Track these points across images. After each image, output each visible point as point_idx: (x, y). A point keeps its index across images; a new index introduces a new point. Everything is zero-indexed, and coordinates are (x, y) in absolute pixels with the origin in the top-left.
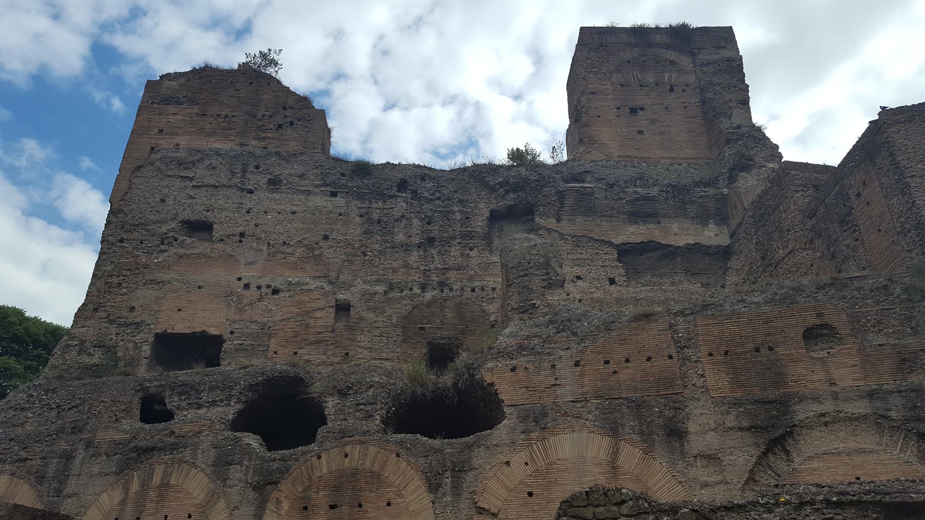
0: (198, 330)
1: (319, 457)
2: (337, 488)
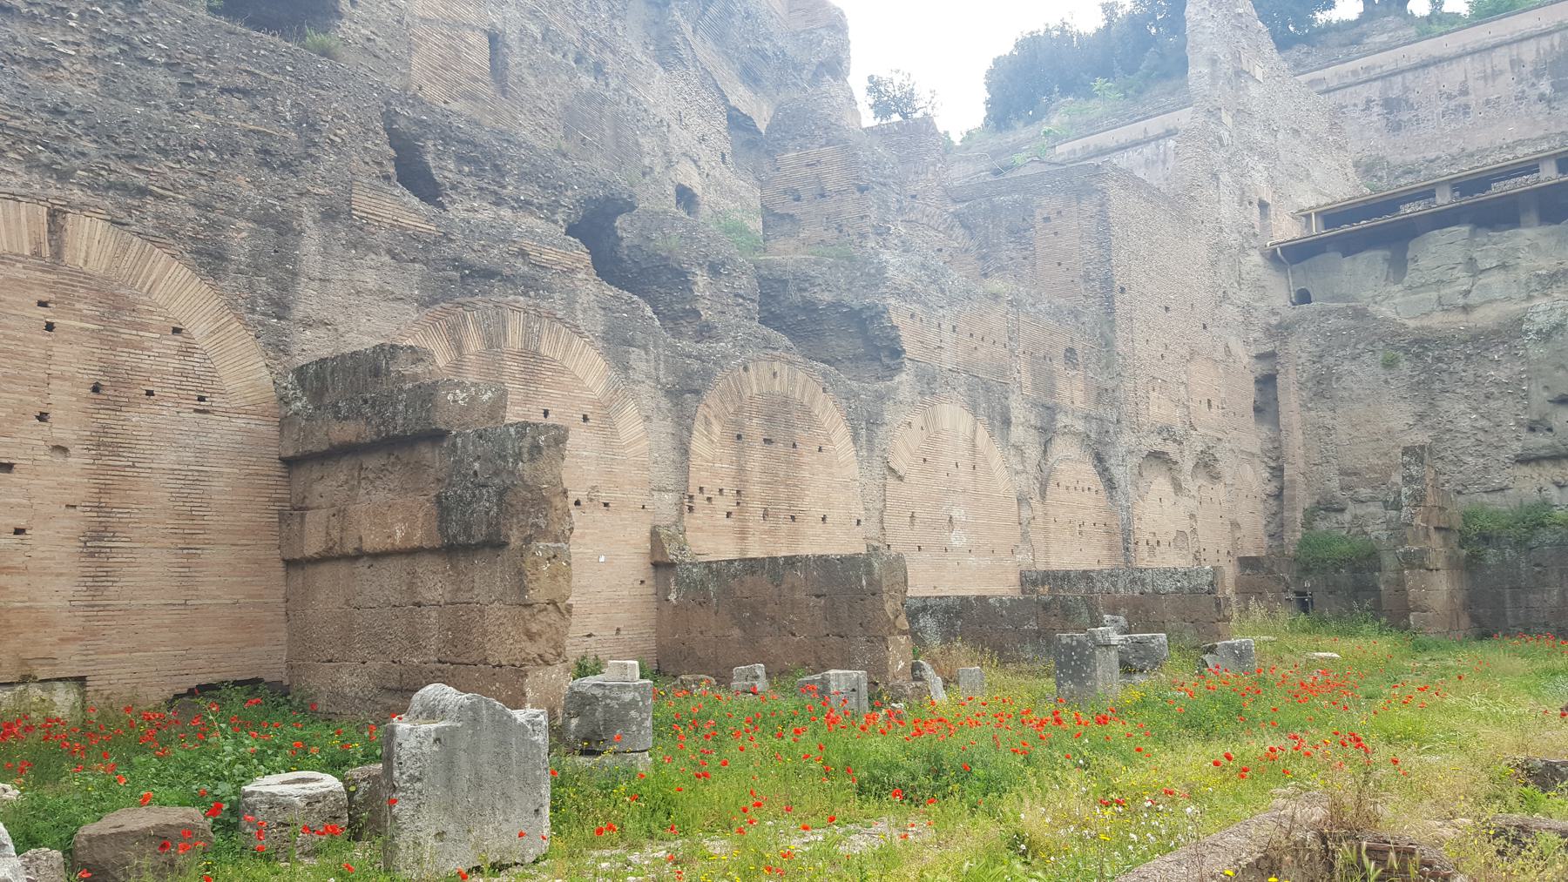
1: (746, 369)
2: (770, 418)
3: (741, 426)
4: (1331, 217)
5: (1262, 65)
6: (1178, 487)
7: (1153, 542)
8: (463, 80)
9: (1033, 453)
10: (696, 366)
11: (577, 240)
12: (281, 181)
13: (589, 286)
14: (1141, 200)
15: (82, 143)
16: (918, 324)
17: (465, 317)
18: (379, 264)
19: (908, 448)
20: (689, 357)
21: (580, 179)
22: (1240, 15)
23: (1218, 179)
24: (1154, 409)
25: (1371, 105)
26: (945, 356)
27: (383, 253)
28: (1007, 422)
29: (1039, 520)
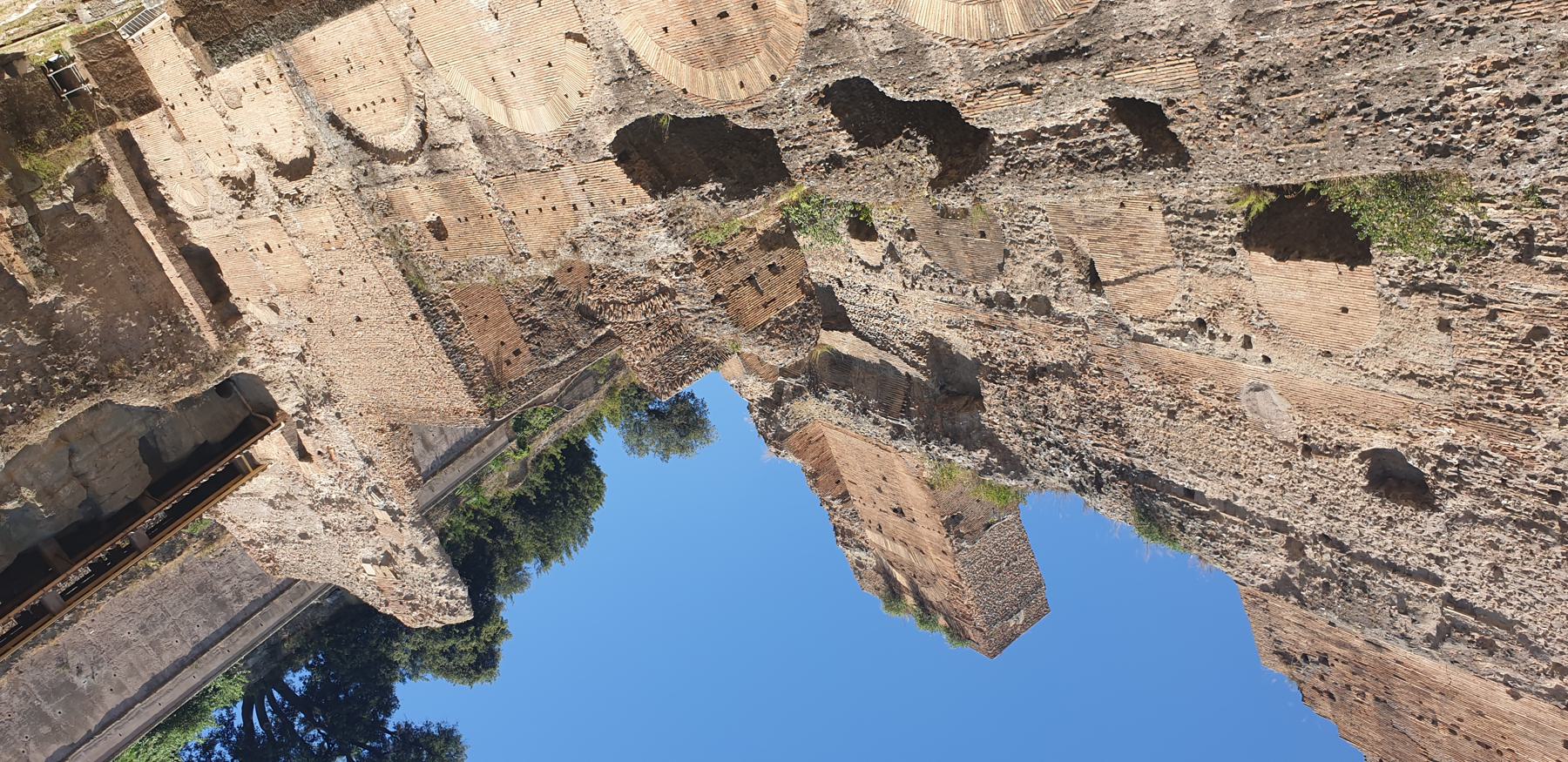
0: (1291, 263)
1: (773, 78)
2: (729, 40)
3: (757, 19)
4: (235, 474)
5: (371, 578)
6: (261, 152)
7: (264, 85)
8: (1112, 234)
9: (436, 121)
10: (825, 60)
11: (979, 127)
12: (1262, 59)
13: (955, 89)
14: (435, 407)
15: (1444, 15)
16: (614, 197)
17: (1063, 6)
18: (1156, 22)
19: (571, 68)
20: (834, 65)
21: (990, 186)
22: (414, 610)
23: (364, 460)
24: (326, 218)
25: (236, 597)
26: (574, 178)
27: (1155, 34)
28: (478, 140)
29: (399, 55)
